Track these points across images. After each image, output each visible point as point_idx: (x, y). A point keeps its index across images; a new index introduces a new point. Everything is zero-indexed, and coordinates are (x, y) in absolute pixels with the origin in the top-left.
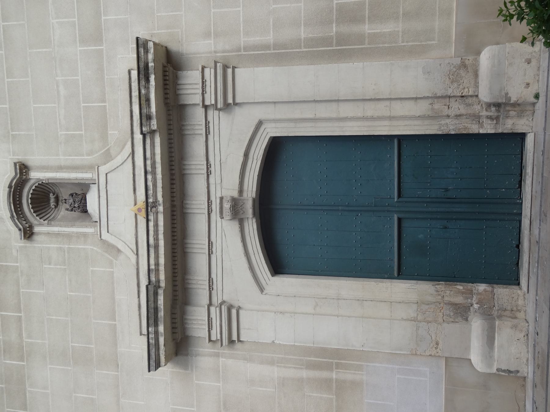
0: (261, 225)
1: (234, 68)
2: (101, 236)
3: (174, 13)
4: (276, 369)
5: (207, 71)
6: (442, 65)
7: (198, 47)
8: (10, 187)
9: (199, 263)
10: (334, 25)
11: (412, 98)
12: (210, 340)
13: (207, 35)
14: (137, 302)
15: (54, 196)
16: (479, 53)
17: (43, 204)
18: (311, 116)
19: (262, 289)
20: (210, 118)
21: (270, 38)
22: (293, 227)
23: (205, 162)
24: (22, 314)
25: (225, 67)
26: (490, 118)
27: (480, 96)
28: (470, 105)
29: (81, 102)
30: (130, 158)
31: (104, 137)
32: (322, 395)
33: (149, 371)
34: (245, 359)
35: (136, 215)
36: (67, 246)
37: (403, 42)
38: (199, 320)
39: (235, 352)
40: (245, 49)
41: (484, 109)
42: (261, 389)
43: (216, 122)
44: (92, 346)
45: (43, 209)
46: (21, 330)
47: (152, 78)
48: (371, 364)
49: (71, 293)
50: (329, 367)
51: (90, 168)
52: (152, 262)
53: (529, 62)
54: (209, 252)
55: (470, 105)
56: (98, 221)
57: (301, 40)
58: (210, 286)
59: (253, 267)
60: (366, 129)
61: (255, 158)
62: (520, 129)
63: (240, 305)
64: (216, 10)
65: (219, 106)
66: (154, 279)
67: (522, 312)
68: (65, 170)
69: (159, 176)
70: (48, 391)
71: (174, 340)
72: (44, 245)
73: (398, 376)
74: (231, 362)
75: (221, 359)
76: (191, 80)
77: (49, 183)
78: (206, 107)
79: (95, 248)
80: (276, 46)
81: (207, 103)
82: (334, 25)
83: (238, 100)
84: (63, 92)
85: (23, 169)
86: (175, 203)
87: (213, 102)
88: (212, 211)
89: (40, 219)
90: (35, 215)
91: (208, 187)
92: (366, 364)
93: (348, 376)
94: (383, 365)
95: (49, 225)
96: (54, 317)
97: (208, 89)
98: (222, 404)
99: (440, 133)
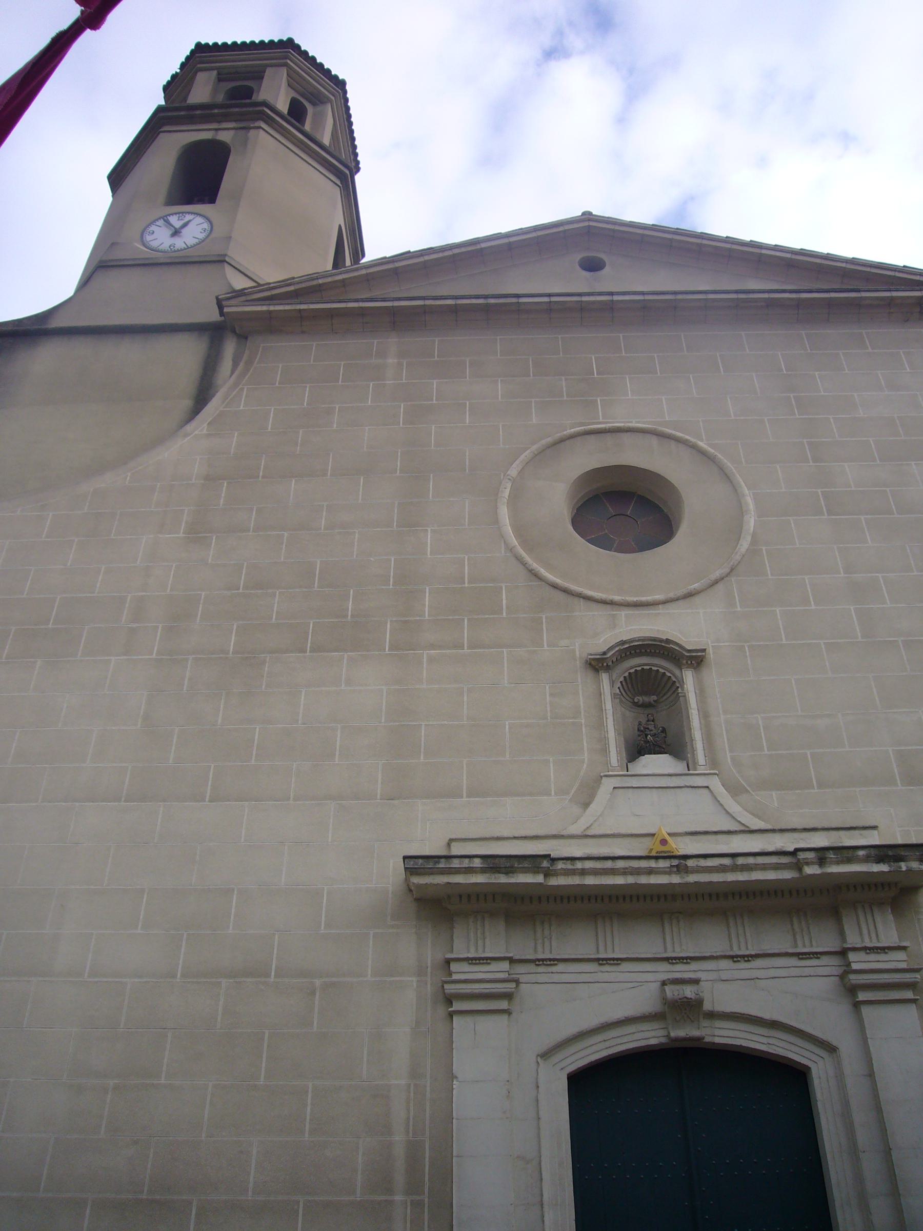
0: (645, 1052)
5: (901, 955)
8: (668, 641)
9: (578, 941)
12: (448, 962)
19: (546, 1055)
20: (825, 960)
23: (753, 953)
24: (466, 650)
32: (360, 1172)
33: (405, 858)
35: (653, 835)
36: (583, 721)
38: (487, 945)
42: (365, 1052)
43: (821, 971)
44: (422, 757)
45: (632, 685)
47: (884, 868)
50: (413, 1187)
51: (713, 762)
52: (589, 865)
54: (603, 959)
58: (543, 960)
61: (771, 1041)
63: (514, 1014)
65: (852, 977)
66: (559, 867)
68: (703, 722)
69: (731, 877)
71: (449, 897)
72: (580, 687)
74: (409, 999)
76: (886, 930)
87: (855, 966)
88: (673, 964)
90: (626, 674)
91: (712, 958)
95: (614, 696)
96: (465, 698)
97: (873, 957)
98: (334, 979)
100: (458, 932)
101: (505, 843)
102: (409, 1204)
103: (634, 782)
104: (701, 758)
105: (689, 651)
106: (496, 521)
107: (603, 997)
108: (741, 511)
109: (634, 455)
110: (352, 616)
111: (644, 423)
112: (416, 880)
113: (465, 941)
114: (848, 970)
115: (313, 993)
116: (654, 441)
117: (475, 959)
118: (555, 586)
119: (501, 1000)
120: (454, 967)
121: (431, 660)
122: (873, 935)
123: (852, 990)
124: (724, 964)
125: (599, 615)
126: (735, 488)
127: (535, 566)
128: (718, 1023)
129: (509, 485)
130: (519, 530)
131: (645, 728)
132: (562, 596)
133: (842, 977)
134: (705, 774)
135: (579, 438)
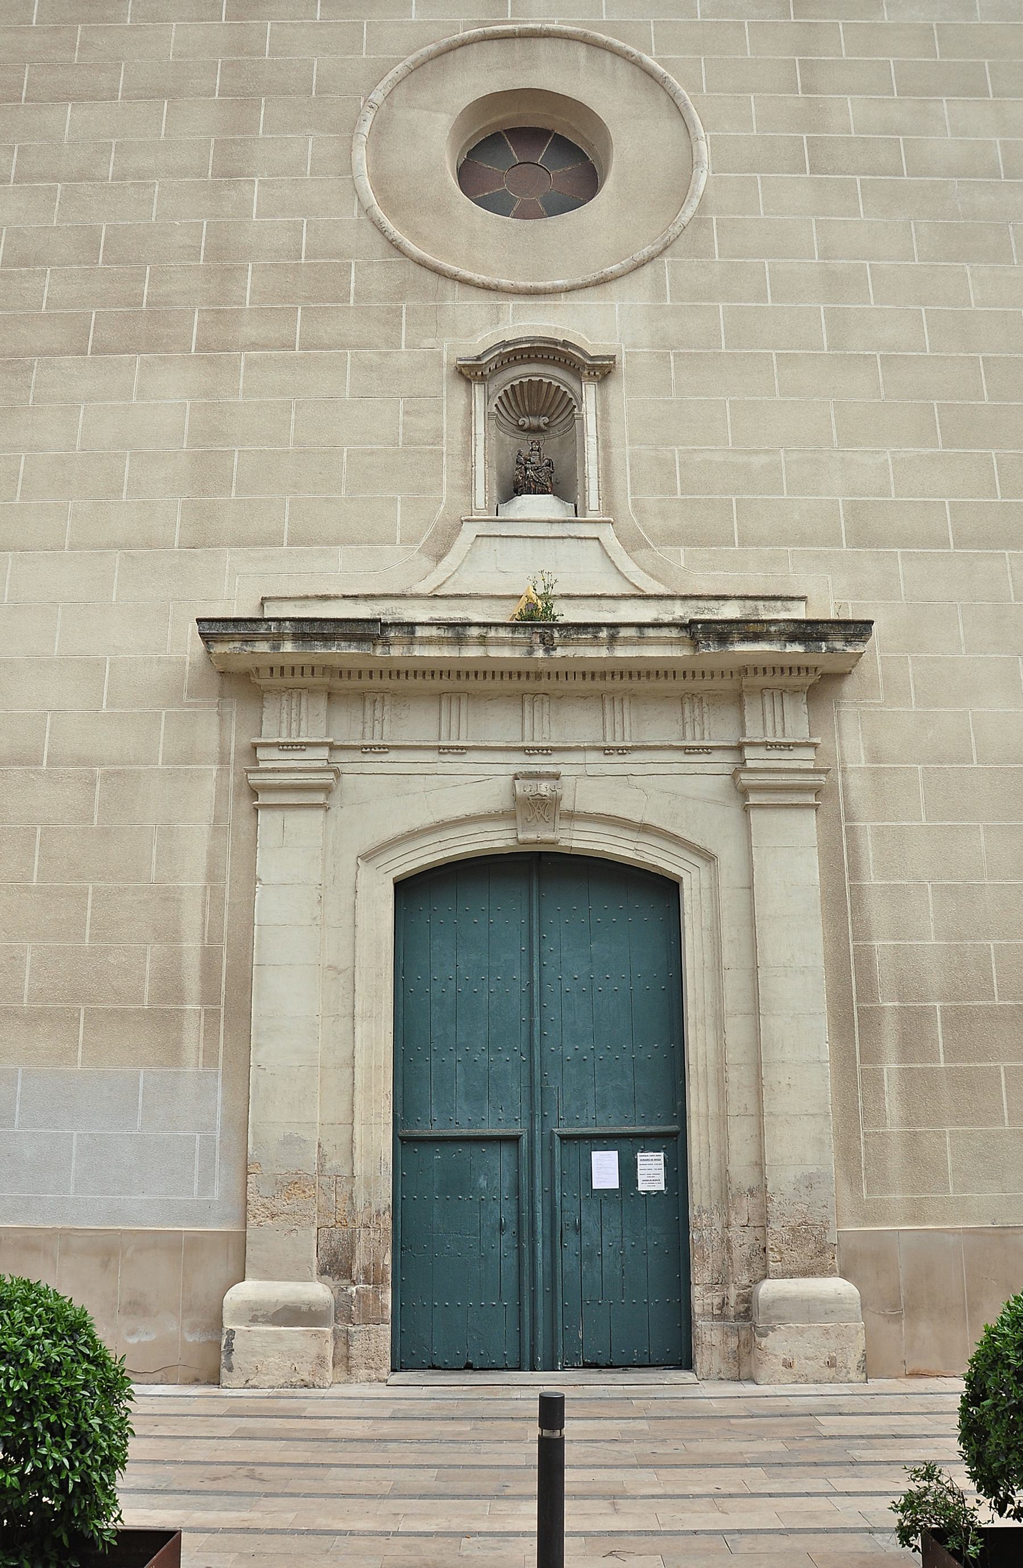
1: (816, 807)
2: (468, 521)
3: (912, 690)
4: (200, 884)
5: (810, 753)
6: (823, 1210)
7: (854, 737)
8: (566, 344)
9: (418, 725)
10: (896, 1004)
11: (761, 1156)
12: (255, 747)
13: (875, 755)
14: (332, 592)
15: (542, 426)
16: (844, 1275)
17: (527, 403)
18: (725, 960)
19: (367, 857)
20: (717, 756)
21: (872, 879)
22: (497, 920)
25: (817, 790)
26: (724, 1304)
27: (768, 1281)
28: (749, 1265)
29: (738, 497)
30: (629, 591)
31: (673, 538)
32: (147, 979)
33: (199, 621)
34: (217, 819)
37: (865, 1134)
39: (231, 797)
40: (850, 830)
41: (742, 1291)
42: (154, 853)
43: (709, 769)
44: (233, 494)
46: (264, 347)
48: (220, 1083)
49: (345, 455)
50: (208, 996)
51: (609, 506)
53: (831, 1364)
55: (749, 1265)
56: (499, 518)
57: (870, 939)
59: (413, 839)
60: (701, 1069)
62: (703, 1358)
64: (920, 773)
65: (743, 776)
66: (392, 635)
67: (347, 1377)
68: (601, 453)
70: (134, 399)
73: (198, 1138)
75: (215, 767)
77: (573, 420)
78: (740, 748)
79: (442, 506)
80: (858, 892)
81: (748, 753)
82: (896, 1004)
83: (755, 815)
84: (758, 461)
85: (602, 371)
86: (545, 679)
87: (750, 764)
88: (530, 754)
89: (500, 398)
90: (508, 387)
92: (220, 1072)
93: (192, 1036)
94: (219, 1108)
95: (489, 416)
96: (293, 417)
97: (775, 754)
99: (693, 1212)
100: (269, 712)
101: (332, 603)
102: (203, 1013)
103: (504, 530)
104: (593, 500)
105: (592, 358)
106: (349, 169)
107: (448, 792)
108: (691, 163)
109: (552, 73)
110: (148, 304)
111: (570, 24)
112: (219, 649)
113: (277, 723)
114: (741, 767)
115: (93, 784)
116: (582, 51)
117: (287, 744)
118: (422, 264)
119: (319, 794)
120: (261, 753)
121: (251, 364)
122: (779, 728)
123: (744, 792)
124: (593, 757)
125: (478, 304)
126: (687, 128)
127: (397, 234)
128: (578, 826)
129: (370, 116)
130: (379, 183)
131: (526, 460)
132: (430, 278)
133: (734, 776)
134: (595, 522)
135: (475, 46)
